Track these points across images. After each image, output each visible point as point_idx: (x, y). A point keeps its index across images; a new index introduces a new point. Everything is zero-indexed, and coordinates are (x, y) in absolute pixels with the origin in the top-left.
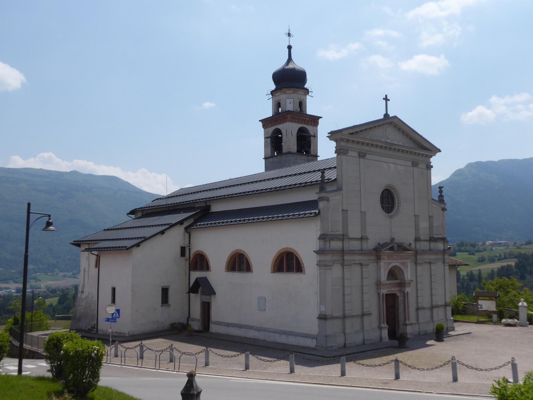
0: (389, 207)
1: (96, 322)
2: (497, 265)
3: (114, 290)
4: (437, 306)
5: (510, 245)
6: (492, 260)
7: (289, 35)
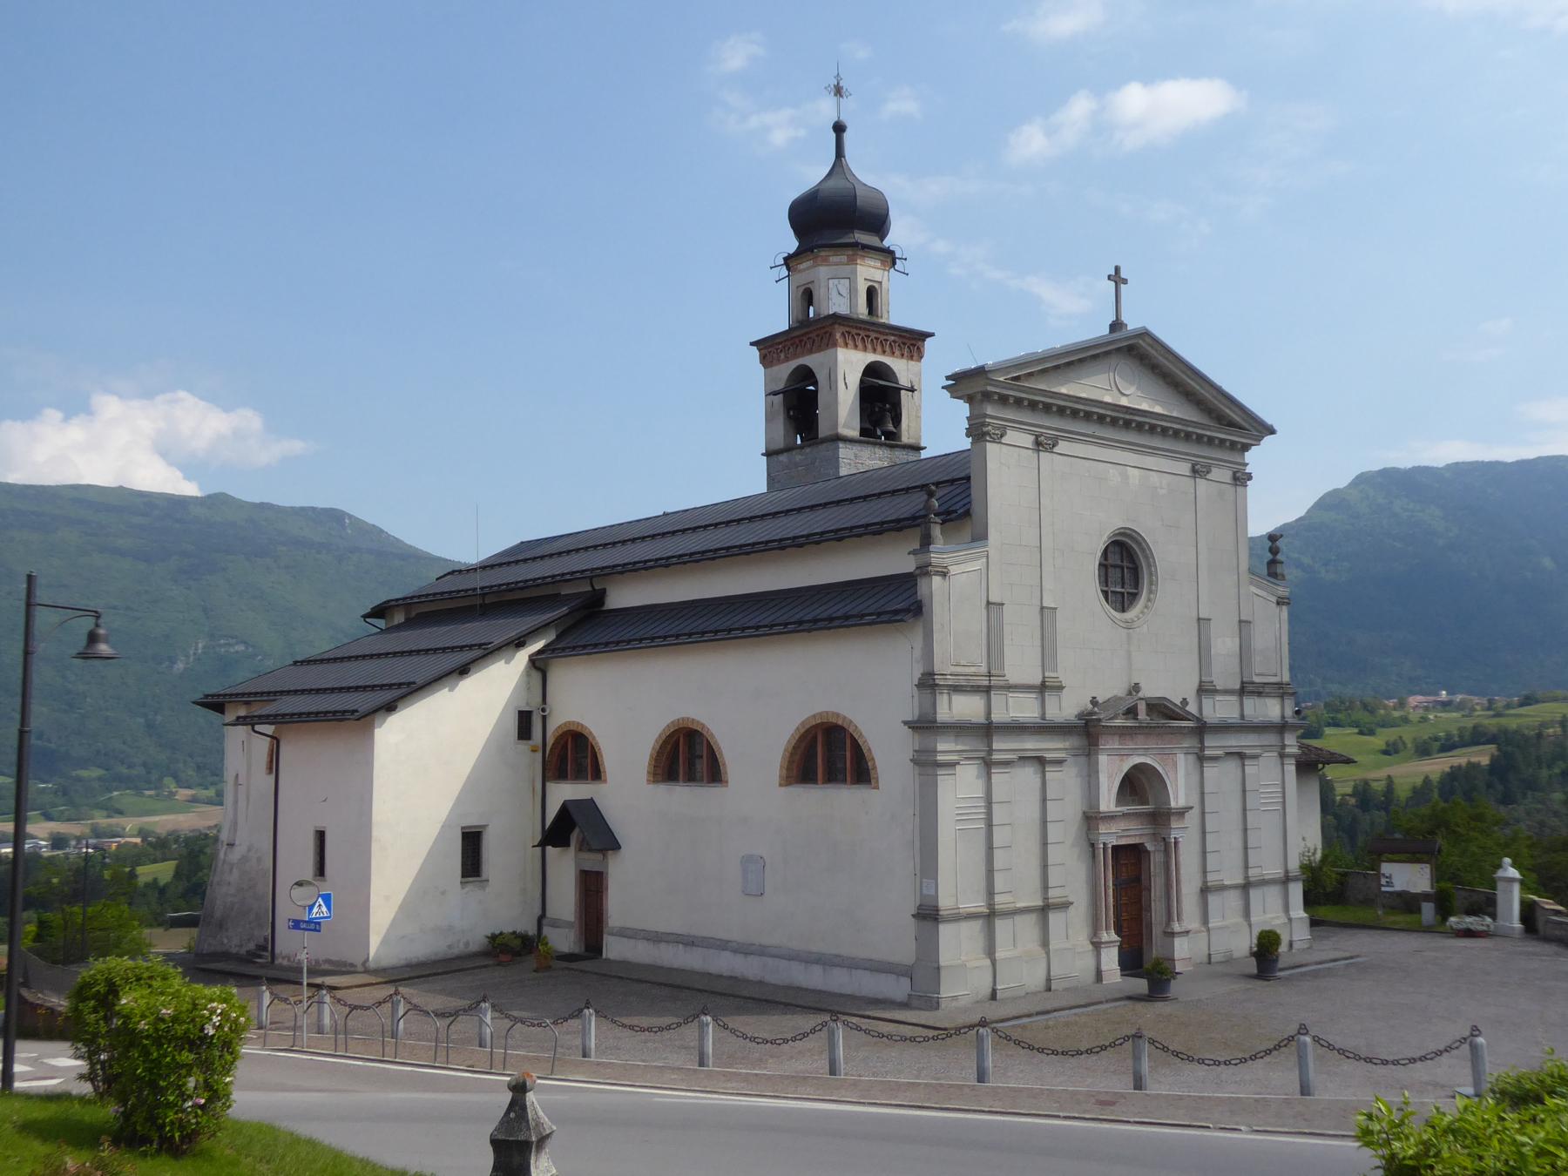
0: (1123, 594)
1: (270, 931)
2: (1436, 764)
3: (321, 836)
4: (1264, 883)
5: (1478, 707)
6: (1423, 751)
7: (838, 91)
